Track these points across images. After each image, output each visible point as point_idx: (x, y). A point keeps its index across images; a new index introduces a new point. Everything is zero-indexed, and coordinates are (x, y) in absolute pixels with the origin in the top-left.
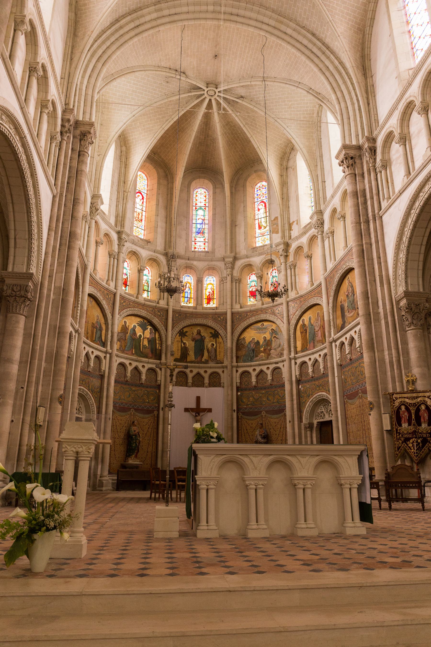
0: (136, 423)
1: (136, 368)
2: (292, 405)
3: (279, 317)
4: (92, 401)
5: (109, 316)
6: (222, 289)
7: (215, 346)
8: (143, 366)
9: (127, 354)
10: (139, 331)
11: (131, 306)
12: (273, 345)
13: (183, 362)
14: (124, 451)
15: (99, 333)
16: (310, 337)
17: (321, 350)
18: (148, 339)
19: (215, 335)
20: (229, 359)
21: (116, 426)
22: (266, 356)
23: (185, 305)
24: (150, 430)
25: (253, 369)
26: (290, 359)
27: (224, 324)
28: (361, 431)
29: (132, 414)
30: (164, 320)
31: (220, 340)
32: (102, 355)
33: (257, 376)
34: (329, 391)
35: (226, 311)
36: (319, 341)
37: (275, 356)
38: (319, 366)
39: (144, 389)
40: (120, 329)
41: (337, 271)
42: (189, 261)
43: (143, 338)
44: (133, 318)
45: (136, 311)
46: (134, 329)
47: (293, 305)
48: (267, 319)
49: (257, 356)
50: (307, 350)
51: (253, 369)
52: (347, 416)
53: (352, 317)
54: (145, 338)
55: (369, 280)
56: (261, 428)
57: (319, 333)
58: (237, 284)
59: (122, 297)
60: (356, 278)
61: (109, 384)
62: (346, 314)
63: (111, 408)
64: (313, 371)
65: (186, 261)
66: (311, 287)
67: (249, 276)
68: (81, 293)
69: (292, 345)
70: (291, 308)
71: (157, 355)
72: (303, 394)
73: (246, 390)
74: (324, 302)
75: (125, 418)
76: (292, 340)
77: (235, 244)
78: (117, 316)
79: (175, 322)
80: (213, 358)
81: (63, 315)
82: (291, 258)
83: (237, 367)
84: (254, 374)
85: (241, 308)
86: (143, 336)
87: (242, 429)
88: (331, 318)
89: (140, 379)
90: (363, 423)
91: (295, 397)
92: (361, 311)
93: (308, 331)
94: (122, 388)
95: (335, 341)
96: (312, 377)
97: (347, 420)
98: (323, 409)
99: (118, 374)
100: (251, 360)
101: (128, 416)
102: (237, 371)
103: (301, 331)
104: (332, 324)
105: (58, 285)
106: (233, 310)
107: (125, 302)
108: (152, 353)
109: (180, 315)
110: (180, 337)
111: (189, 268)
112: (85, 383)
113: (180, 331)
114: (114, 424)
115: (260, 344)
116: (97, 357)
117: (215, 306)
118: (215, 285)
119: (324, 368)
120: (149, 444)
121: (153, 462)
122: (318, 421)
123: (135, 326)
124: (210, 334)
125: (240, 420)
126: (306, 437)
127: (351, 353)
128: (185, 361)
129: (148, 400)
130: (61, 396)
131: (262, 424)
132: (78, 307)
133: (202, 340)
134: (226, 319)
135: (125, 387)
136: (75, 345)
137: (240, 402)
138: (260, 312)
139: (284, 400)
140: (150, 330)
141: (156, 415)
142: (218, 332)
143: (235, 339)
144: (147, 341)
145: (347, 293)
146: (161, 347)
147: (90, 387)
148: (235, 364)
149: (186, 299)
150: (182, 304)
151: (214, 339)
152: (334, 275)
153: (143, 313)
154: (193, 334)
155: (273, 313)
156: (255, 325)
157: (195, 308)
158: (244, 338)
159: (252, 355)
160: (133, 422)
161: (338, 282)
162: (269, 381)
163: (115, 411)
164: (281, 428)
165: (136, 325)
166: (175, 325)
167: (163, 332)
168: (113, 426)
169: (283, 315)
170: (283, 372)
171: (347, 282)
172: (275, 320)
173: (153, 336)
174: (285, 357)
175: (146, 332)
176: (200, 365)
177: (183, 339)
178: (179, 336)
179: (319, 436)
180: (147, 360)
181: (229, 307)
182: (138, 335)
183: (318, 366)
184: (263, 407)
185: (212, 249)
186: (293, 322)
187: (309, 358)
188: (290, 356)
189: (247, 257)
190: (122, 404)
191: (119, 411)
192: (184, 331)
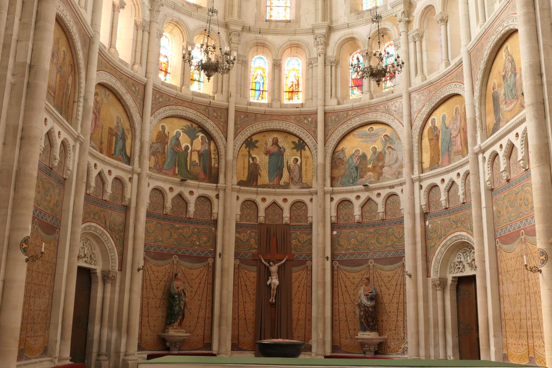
0: (179, 275)
1: (180, 195)
2: (415, 250)
3: (396, 116)
4: (111, 244)
5: (136, 117)
6: (310, 76)
7: (299, 163)
8: (191, 193)
9: (166, 174)
10: (185, 141)
11: (172, 103)
12: (387, 159)
13: (252, 186)
14: (163, 317)
15: (120, 143)
16: (441, 147)
17: (461, 166)
18: (198, 152)
19: (300, 145)
21: (150, 280)
22: (376, 177)
23: (255, 101)
24: (202, 285)
25: (356, 195)
26: (413, 182)
27: (313, 129)
28: (523, 296)
30: (222, 124)
31: (307, 152)
32: (125, 177)
33: (363, 207)
34: (472, 231)
35: (315, 109)
36: (457, 153)
37: (390, 177)
38: (457, 191)
39: (192, 227)
40: (155, 138)
41: (487, 38)
42: (260, 35)
43: (191, 151)
44: (175, 121)
46: (177, 138)
47: (418, 97)
48: (378, 120)
49: (362, 177)
50: (439, 166)
51: (356, 195)
52: (500, 270)
53: (511, 110)
54: (195, 150)
55: (543, 44)
56: (366, 285)
57: (458, 140)
58: (333, 68)
59: (157, 91)
60: (520, 49)
61: (136, 219)
62: (501, 106)
63: (141, 254)
64: (448, 200)
65: (257, 35)
66: (446, 68)
67: (351, 57)
68: (83, 81)
69: (416, 159)
70: (415, 102)
71: (213, 176)
72: (431, 235)
73: (345, 227)
74: (465, 90)
75: (162, 269)
76: (416, 152)
77: (331, 8)
78: (148, 117)
79: (239, 126)
80: (296, 179)
81: (29, 109)
82: (415, 25)
83: (332, 193)
84: (357, 204)
85: (339, 104)
86: (190, 148)
87: (339, 286)
88: (477, 114)
89: (187, 211)
90: (527, 282)
91: (419, 239)
92: (528, 99)
93: (440, 137)
94: (159, 225)
95: (483, 152)
96: (446, 208)
97: (500, 277)
98: (462, 257)
99: (151, 204)
100: (353, 183)
101: (169, 265)
102: (332, 199)
103: (430, 137)
104: (478, 124)
105: (20, 59)
106: (326, 107)
107: (162, 96)
108: (205, 173)
109: (247, 116)
110: (248, 149)
111: (261, 46)
112: (99, 218)
113: (247, 140)
115: (366, 159)
116: (117, 179)
117: (300, 101)
118: (300, 71)
119: (465, 194)
120: (200, 306)
121: (206, 332)
122: (454, 275)
123: (178, 134)
124: (292, 144)
125: (335, 272)
126: (435, 299)
127: (508, 169)
128: (254, 184)
129: (200, 243)
130: (26, 240)
131: (368, 279)
132: (79, 101)
133: (281, 153)
134: (316, 122)
135: (162, 222)
136: (74, 161)
139: (402, 243)
140: (202, 139)
141: (211, 265)
142: (304, 141)
143: (330, 151)
144: (197, 156)
145: (503, 73)
146: (218, 163)
147: (108, 223)
148: (328, 188)
149: (258, 93)
150: (252, 100)
151: (297, 151)
152: (482, 46)
153: (191, 113)
154: (266, 144)
155: (388, 111)
156: (360, 130)
157: (269, 105)
158: (343, 150)
159: (354, 175)
160: (176, 275)
161: (490, 56)
162: (381, 214)
164: (396, 285)
165: (181, 131)
166: (239, 131)
167: (221, 142)
169: (402, 113)
170: (401, 200)
171: (504, 54)
172: (389, 122)
173: (207, 148)
174: (405, 177)
175: (194, 141)
176: (277, 190)
177: (251, 152)
178: (246, 148)
179: (455, 298)
180: (197, 183)
182: (183, 146)
183: (455, 191)
184: (371, 254)
185: (296, 17)
186: (418, 123)
187: (440, 178)
188: (413, 177)
189: (348, 26)
190: (159, 248)
192: (254, 140)
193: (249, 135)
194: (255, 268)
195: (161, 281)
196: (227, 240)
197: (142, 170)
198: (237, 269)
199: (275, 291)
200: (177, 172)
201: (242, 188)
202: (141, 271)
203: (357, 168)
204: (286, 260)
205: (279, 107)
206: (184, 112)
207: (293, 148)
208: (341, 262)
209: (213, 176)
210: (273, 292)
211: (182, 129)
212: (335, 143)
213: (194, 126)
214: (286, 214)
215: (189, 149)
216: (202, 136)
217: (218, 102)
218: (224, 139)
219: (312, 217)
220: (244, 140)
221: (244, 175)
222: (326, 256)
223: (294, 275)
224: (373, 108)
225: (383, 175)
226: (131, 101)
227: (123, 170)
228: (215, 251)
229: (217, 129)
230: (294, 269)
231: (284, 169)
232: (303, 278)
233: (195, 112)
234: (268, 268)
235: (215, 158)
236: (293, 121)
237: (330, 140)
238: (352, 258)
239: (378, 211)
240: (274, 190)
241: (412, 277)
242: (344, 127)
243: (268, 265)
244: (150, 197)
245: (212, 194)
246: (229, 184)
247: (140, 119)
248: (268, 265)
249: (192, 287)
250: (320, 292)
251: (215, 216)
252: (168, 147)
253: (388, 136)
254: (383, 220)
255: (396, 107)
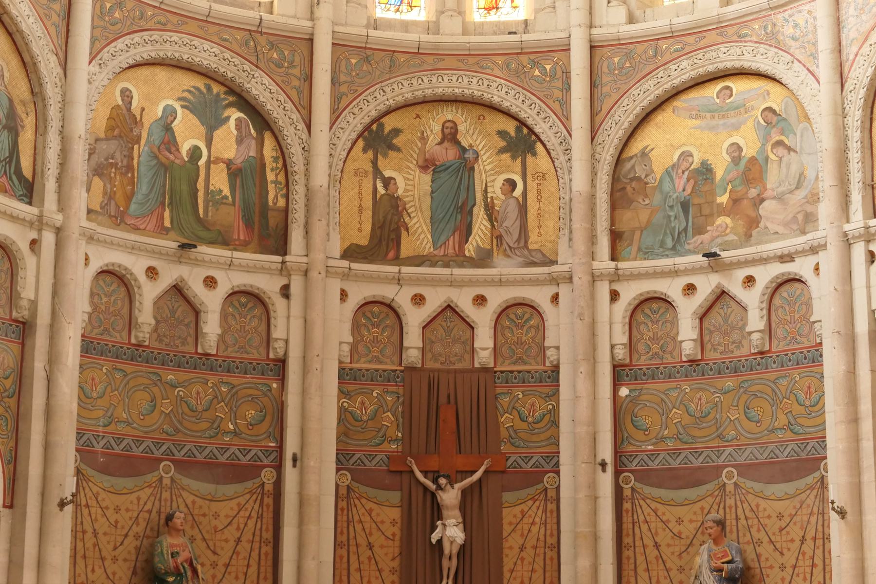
0: (178, 520)
1: (178, 290)
2: (855, 439)
8: (210, 282)
9: (136, 229)
10: (188, 134)
12: (773, 178)
13: (384, 261)
18: (229, 163)
19: (522, 142)
20: (580, 244)
21: (95, 533)
22: (741, 230)
23: (391, 15)
24: (245, 546)
25: (682, 283)
26: (847, 242)
27: (558, 94)
29: (167, 481)
31: (540, 162)
33: (703, 317)
35: (564, 35)
37: (781, 229)
39: (212, 380)
43: (209, 162)
44: (161, 74)
45: (175, 45)
48: (746, 65)
49: (700, 230)
51: (682, 283)
54: (218, 160)
56: (716, 541)
71: (270, 234)
75: (128, 502)
79: (344, 89)
83: (616, 277)
84: (687, 310)
85: (631, 20)
100: (674, 248)
101: (148, 491)
102: (614, 296)
106: (594, 31)
108: (249, 225)
109: (367, 60)
110: (370, 154)
113: (368, 128)
114: (88, 527)
115: (713, 179)
125: (627, 506)
128: (391, 254)
131: (721, 523)
134: (567, 74)
135: (129, 368)
137: (630, 427)
138: (712, 37)
139: (818, 421)
140: (238, 127)
141: (269, 487)
142: (531, 131)
143: (607, 156)
144: (224, 175)
148: (604, 263)
151: (514, 158)
153: (206, 54)
154: (423, 139)
155: (773, 40)
156: (693, 95)
157: (432, 27)
158: (644, 154)
159: (678, 225)
160: (169, 518)
162: (755, 336)
163: (89, 472)
164: (803, 540)
167: (292, 135)
168: (77, 533)
169: (815, 44)
170: (814, 295)
173: (252, 153)
174: (825, 228)
175: (218, 134)
176: (457, 271)
178: (365, 150)
180: (228, 253)
181: (578, 17)
182: (185, 148)
191: (104, 470)
192: (387, 130)
193: (374, 114)
194: (395, 497)
195: (126, 536)
196: (315, 416)
197: (66, 218)
198: (344, 498)
199: (455, 561)
200: (167, 224)
201: (355, 266)
202: (69, 509)
203: (685, 206)
204: (486, 472)
205: (460, 31)
206: (185, 49)
207: (502, 151)
208: (644, 476)
209: (270, 234)
210: (450, 565)
211: (180, 99)
212: (621, 133)
213: (216, 88)
214: (484, 340)
215: (200, 157)
216: (238, 120)
217: (283, 20)
218: (301, 126)
219: (558, 348)
220: (360, 128)
221: (360, 230)
222: (599, 460)
223: (509, 515)
224: (731, 31)
225: (762, 225)
226: (31, 20)
227: (13, 218)
228: (281, 448)
229: (282, 97)
230: (508, 497)
231: (475, 210)
232: (533, 523)
233: (216, 49)
234: (433, 495)
235: (276, 182)
236: (497, 72)
237: (606, 125)
238: (675, 464)
239: (748, 329)
240: (447, 271)
241: (849, 517)
242: (646, 86)
243: (433, 487)
244: (92, 295)
245: (268, 285)
246: (318, 256)
247: (59, 70)
248: (433, 487)
249: (215, 553)
250: (584, 562)
251: (278, 348)
252: (141, 152)
253: (774, 112)
254: (761, 353)
255: (796, 25)
